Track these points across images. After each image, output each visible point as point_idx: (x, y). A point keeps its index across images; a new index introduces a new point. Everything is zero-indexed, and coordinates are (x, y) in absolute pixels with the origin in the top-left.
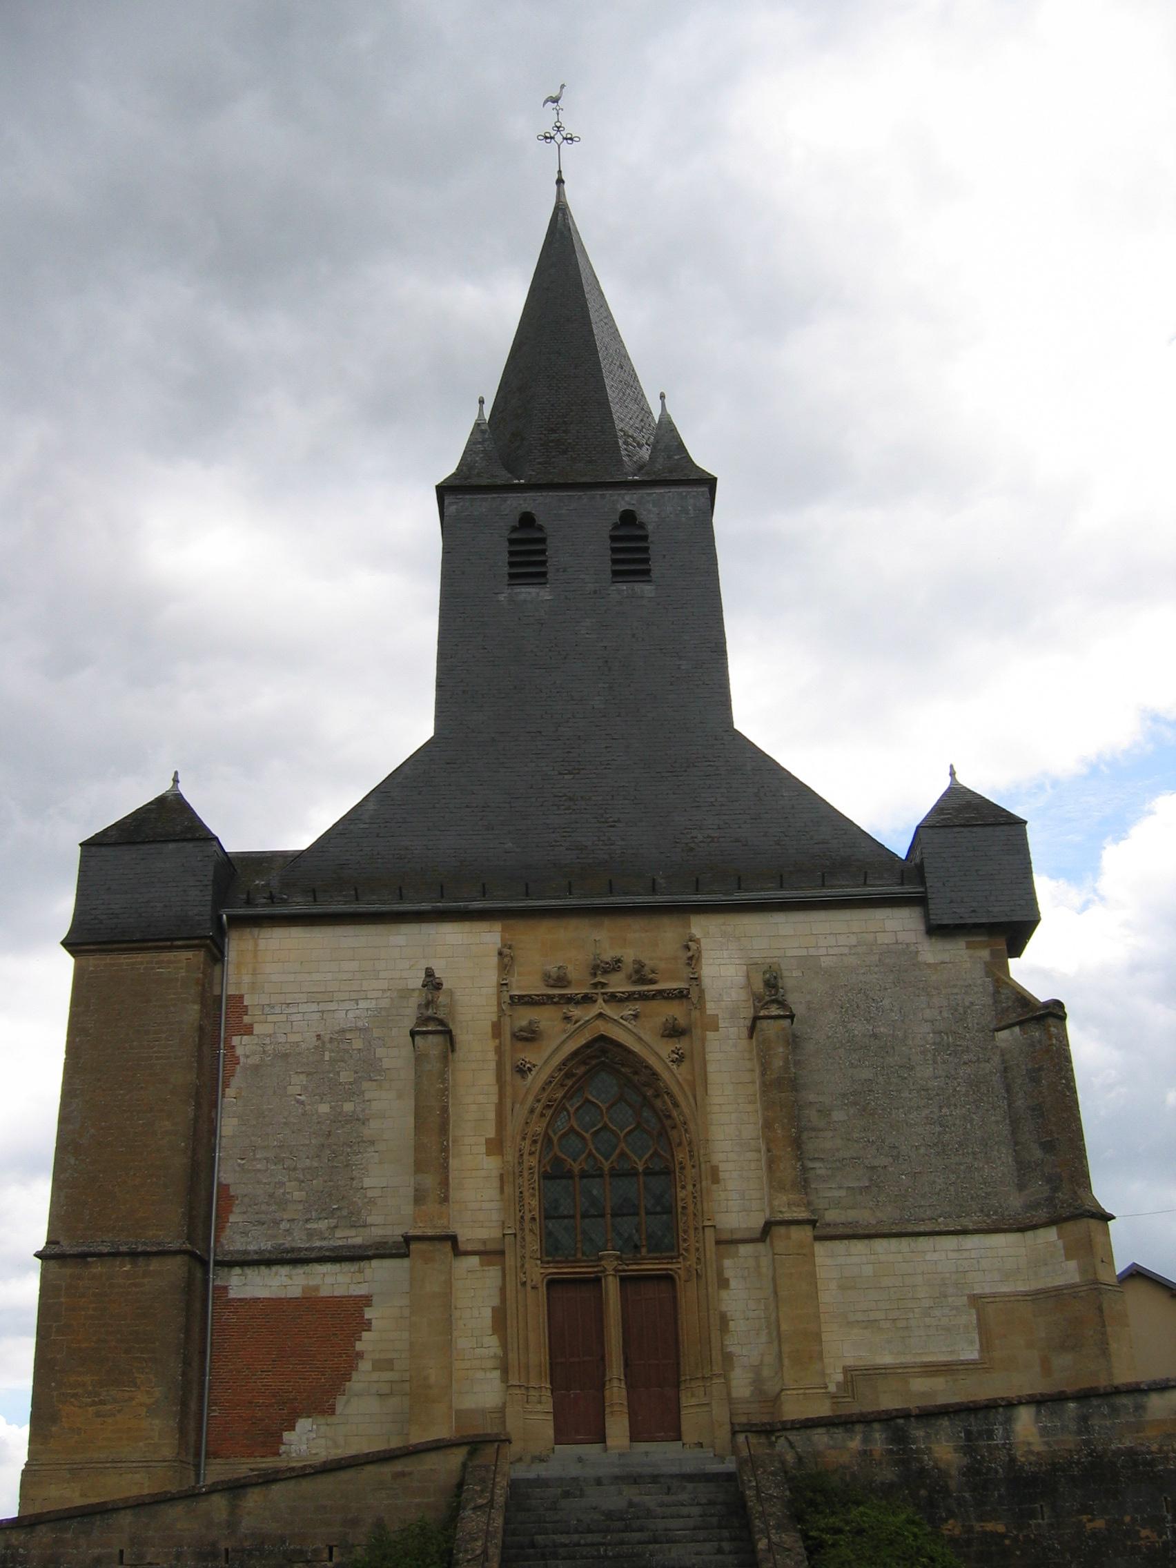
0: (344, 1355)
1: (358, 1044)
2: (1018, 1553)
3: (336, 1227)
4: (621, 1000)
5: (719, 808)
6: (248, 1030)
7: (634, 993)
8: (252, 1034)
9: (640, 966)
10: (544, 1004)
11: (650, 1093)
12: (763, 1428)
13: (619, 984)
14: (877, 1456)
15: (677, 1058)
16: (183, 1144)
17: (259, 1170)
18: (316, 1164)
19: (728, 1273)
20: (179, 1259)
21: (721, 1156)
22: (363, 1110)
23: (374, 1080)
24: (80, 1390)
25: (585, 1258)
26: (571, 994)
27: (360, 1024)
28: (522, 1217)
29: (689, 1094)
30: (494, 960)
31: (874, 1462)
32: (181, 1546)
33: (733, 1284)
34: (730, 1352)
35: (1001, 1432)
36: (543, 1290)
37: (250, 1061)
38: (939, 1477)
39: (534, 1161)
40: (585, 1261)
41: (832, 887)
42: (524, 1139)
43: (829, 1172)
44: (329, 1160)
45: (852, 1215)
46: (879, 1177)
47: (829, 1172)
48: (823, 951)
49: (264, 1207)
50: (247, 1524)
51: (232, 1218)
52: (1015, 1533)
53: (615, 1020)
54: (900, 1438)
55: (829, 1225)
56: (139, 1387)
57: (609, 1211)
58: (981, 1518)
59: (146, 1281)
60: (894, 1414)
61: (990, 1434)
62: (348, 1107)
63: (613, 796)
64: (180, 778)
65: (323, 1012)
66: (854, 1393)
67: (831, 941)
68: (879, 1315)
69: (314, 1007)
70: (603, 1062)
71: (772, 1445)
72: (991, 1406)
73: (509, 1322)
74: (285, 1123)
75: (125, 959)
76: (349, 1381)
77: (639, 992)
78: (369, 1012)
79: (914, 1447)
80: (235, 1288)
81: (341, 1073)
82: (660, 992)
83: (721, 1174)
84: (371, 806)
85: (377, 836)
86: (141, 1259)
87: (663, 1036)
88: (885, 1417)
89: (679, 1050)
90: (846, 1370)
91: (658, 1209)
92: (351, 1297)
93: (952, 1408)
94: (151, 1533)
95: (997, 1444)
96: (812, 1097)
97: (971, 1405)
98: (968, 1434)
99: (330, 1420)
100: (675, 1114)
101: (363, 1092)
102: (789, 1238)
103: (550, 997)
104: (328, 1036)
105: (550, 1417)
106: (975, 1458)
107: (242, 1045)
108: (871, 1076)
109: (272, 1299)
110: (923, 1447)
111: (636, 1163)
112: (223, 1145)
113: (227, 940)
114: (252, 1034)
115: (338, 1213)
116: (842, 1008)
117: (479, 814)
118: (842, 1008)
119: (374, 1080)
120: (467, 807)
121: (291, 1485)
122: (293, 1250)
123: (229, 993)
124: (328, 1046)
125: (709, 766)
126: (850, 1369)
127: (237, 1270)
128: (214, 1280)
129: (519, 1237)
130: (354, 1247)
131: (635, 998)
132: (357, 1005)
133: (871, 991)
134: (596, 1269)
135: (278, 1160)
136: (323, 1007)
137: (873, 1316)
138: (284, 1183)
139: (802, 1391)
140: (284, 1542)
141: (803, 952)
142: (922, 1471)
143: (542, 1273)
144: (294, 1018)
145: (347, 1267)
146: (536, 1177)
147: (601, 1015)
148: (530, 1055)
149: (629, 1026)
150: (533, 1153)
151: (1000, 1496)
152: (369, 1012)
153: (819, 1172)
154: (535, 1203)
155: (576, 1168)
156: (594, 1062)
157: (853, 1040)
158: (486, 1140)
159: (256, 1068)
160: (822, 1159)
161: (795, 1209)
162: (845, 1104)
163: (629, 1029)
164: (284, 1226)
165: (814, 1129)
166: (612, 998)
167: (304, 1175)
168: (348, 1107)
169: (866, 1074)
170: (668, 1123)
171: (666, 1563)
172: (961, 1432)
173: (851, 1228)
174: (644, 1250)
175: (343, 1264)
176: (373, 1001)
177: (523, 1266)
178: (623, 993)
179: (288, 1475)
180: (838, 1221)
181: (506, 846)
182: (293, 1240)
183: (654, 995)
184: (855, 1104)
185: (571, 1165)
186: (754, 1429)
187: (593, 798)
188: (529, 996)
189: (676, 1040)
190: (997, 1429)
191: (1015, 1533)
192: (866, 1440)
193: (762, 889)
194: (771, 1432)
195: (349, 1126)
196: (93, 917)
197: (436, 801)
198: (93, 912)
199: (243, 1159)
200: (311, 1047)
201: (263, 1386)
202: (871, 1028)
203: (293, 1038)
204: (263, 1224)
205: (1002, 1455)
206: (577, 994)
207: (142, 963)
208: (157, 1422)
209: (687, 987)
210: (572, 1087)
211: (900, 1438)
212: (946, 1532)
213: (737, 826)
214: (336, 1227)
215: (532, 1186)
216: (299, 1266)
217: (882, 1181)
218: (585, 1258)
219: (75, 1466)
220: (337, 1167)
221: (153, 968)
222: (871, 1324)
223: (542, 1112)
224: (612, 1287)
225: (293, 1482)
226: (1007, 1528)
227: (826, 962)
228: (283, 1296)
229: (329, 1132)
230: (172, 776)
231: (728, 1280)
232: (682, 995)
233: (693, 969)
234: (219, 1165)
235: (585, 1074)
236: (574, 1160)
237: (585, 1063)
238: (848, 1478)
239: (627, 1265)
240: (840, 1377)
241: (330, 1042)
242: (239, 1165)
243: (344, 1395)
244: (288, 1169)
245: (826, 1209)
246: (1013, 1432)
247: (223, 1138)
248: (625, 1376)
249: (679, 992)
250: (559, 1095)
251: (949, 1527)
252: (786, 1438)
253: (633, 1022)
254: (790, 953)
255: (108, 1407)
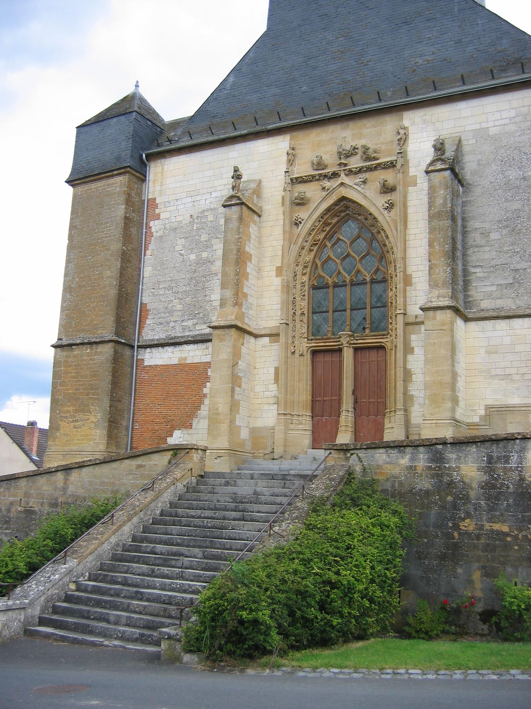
0: (198, 396)
1: (211, 218)
2: (516, 548)
3: (196, 324)
4: (356, 173)
5: (434, 40)
6: (158, 217)
7: (363, 167)
8: (160, 219)
9: (366, 149)
10: (311, 181)
11: (375, 231)
12: (341, 448)
13: (355, 162)
14: (419, 471)
15: (387, 207)
16: (115, 283)
17: (161, 295)
18: (188, 289)
19: (413, 344)
20: (111, 345)
21: (414, 268)
22: (212, 256)
23: (218, 238)
24: (68, 415)
25: (333, 337)
26: (325, 173)
27: (212, 206)
28: (294, 313)
29: (393, 229)
30: (285, 158)
31: (416, 475)
32: (44, 499)
33: (416, 350)
34: (412, 395)
35: (515, 458)
36: (308, 356)
37: (158, 234)
38: (462, 488)
39: (305, 279)
40: (332, 338)
41: (499, 78)
42: (297, 265)
43: (486, 275)
44: (194, 286)
45: (499, 303)
46: (520, 276)
47: (486, 275)
48: (491, 124)
49: (163, 315)
50: (71, 489)
51: (148, 322)
52: (516, 533)
53: (350, 186)
54: (438, 458)
55: (483, 310)
56: (91, 413)
57: (349, 307)
58: (490, 520)
59: (95, 357)
60: (434, 441)
61: (507, 459)
62: (205, 255)
63: (367, 46)
64: (139, 84)
65: (194, 202)
66: (490, 423)
67: (497, 116)
68: (514, 371)
69: (190, 200)
70: (348, 214)
71: (347, 459)
72: (510, 439)
73: (280, 376)
74: (174, 267)
75: (93, 186)
76: (200, 410)
77: (366, 167)
78: (217, 199)
79: (447, 466)
80: (147, 360)
81: (202, 236)
82: (379, 164)
83: (413, 279)
84: (231, 79)
85: (234, 96)
86: (94, 345)
87: (381, 193)
88: (428, 443)
89: (389, 201)
90: (487, 407)
91: (379, 305)
92: (202, 363)
93: (478, 439)
94: (32, 491)
95: (512, 467)
96: (477, 225)
97: (493, 437)
98: (490, 460)
99: (190, 431)
100: (387, 242)
101: (212, 245)
102: (434, 318)
103: (313, 176)
104: (196, 215)
105: (310, 433)
106: (492, 476)
107: (155, 225)
108: (519, 207)
109: (164, 365)
110: (454, 466)
111: (365, 276)
112: (144, 282)
113: (148, 168)
114: (160, 219)
115: (198, 316)
116: (502, 161)
117: (289, 72)
118: (502, 161)
119: (218, 238)
120: (282, 69)
121: (90, 469)
122: (175, 337)
123: (149, 198)
124: (196, 221)
125: (429, 14)
126: (489, 407)
127: (148, 350)
128: (137, 356)
129: (291, 325)
130: (205, 334)
131: (364, 171)
132: (211, 195)
133: (524, 147)
134: (338, 343)
135: (170, 288)
136: (194, 199)
137: (508, 371)
138: (172, 301)
139: (434, 422)
140: (85, 501)
141: (478, 126)
142: (451, 484)
143: (307, 347)
144: (179, 207)
145: (201, 346)
146: (306, 288)
147: (342, 184)
148: (303, 214)
149: (359, 189)
150: (305, 274)
151: (508, 505)
152: (217, 199)
153: (479, 275)
154: (305, 304)
155: (330, 282)
156: (343, 215)
157: (508, 183)
158: (276, 267)
159: (161, 237)
160: (482, 266)
161: (441, 299)
162: (500, 228)
163: (359, 191)
164: (172, 324)
165: (477, 246)
166: (350, 173)
167: (182, 296)
168: (205, 255)
169: (516, 205)
170: (385, 249)
171: (231, 535)
172: (484, 457)
173: (498, 312)
174: (367, 331)
175: (198, 344)
176: (219, 192)
177: (293, 342)
178: (356, 168)
179: (89, 464)
180: (489, 308)
181: (302, 89)
182: (176, 332)
183: (375, 167)
184: (507, 226)
185: (327, 280)
186: (335, 448)
187: (356, 49)
188: (301, 177)
189: (389, 194)
190: (513, 456)
191: (516, 533)
192: (412, 459)
193: (452, 87)
194: (348, 450)
195: (204, 266)
196: (80, 166)
197: (265, 69)
198: (80, 163)
199: (154, 289)
200: (188, 222)
201: (159, 412)
202: (522, 173)
203: (179, 219)
204: (162, 324)
205: (515, 476)
206: (328, 173)
207: (100, 187)
208: (98, 431)
209: (396, 159)
210: (329, 231)
211: (438, 458)
212: (463, 528)
213: (445, 50)
214: (196, 324)
215: (303, 294)
216: (177, 346)
217: (522, 280)
218: (333, 337)
219: (65, 453)
220: (198, 290)
221: (105, 188)
222: (506, 377)
223: (310, 248)
224: (348, 355)
225: (92, 467)
226: (510, 529)
227: (493, 131)
228: (169, 364)
229: (195, 270)
230: (135, 83)
231: (413, 348)
232: (392, 165)
233: (401, 147)
234: (142, 292)
235: (337, 222)
236: (330, 277)
237: (336, 215)
238: (396, 485)
239: (357, 340)
240: (482, 412)
241: (197, 219)
242: (152, 292)
243: (197, 418)
244: (175, 293)
245: (482, 300)
246: (525, 458)
247: (145, 279)
248: (355, 409)
249: (390, 163)
250: (322, 236)
251: (466, 525)
252: (357, 455)
253: (362, 186)
254: (468, 128)
255: (79, 423)
